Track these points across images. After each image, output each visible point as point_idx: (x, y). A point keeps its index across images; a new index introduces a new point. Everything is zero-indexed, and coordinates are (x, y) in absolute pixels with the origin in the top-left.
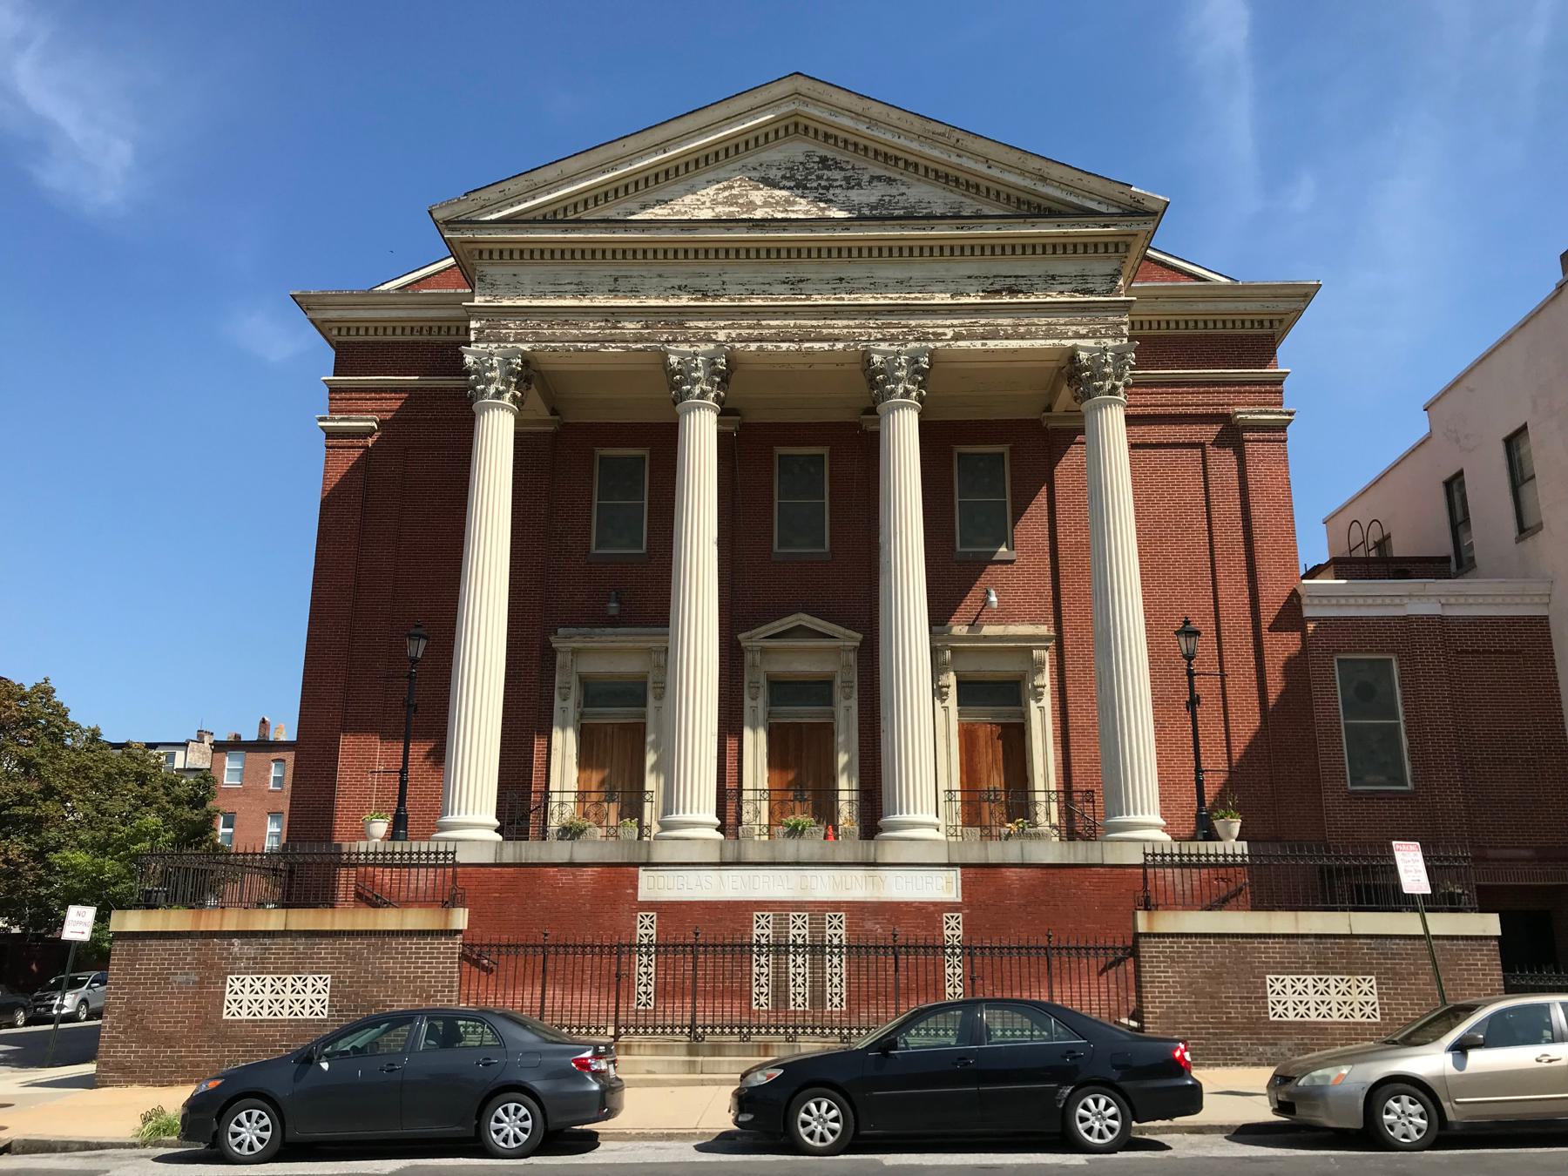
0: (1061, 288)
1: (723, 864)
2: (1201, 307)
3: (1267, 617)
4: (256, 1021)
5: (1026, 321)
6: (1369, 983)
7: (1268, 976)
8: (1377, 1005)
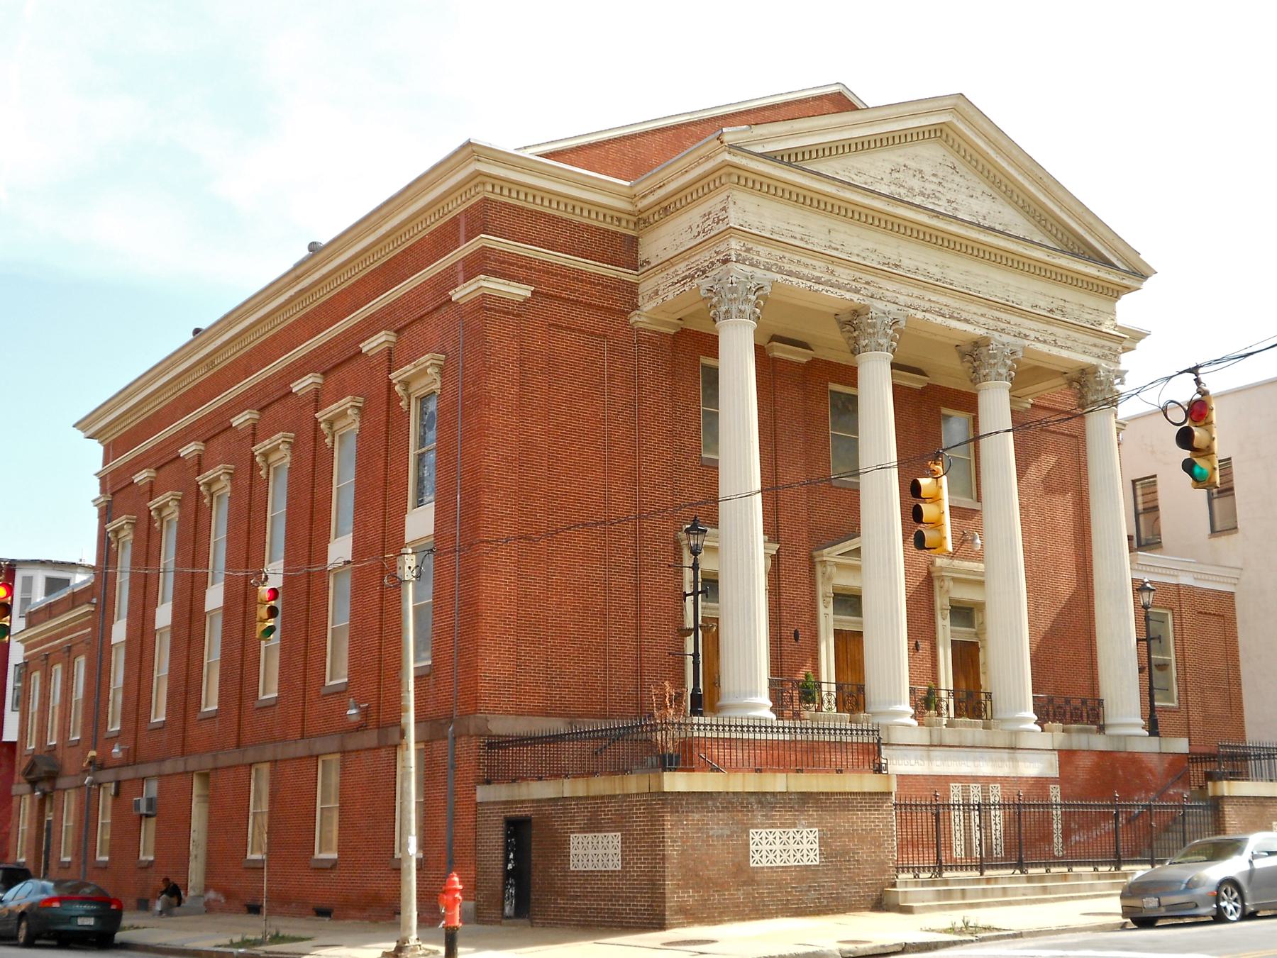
4: (772, 868)
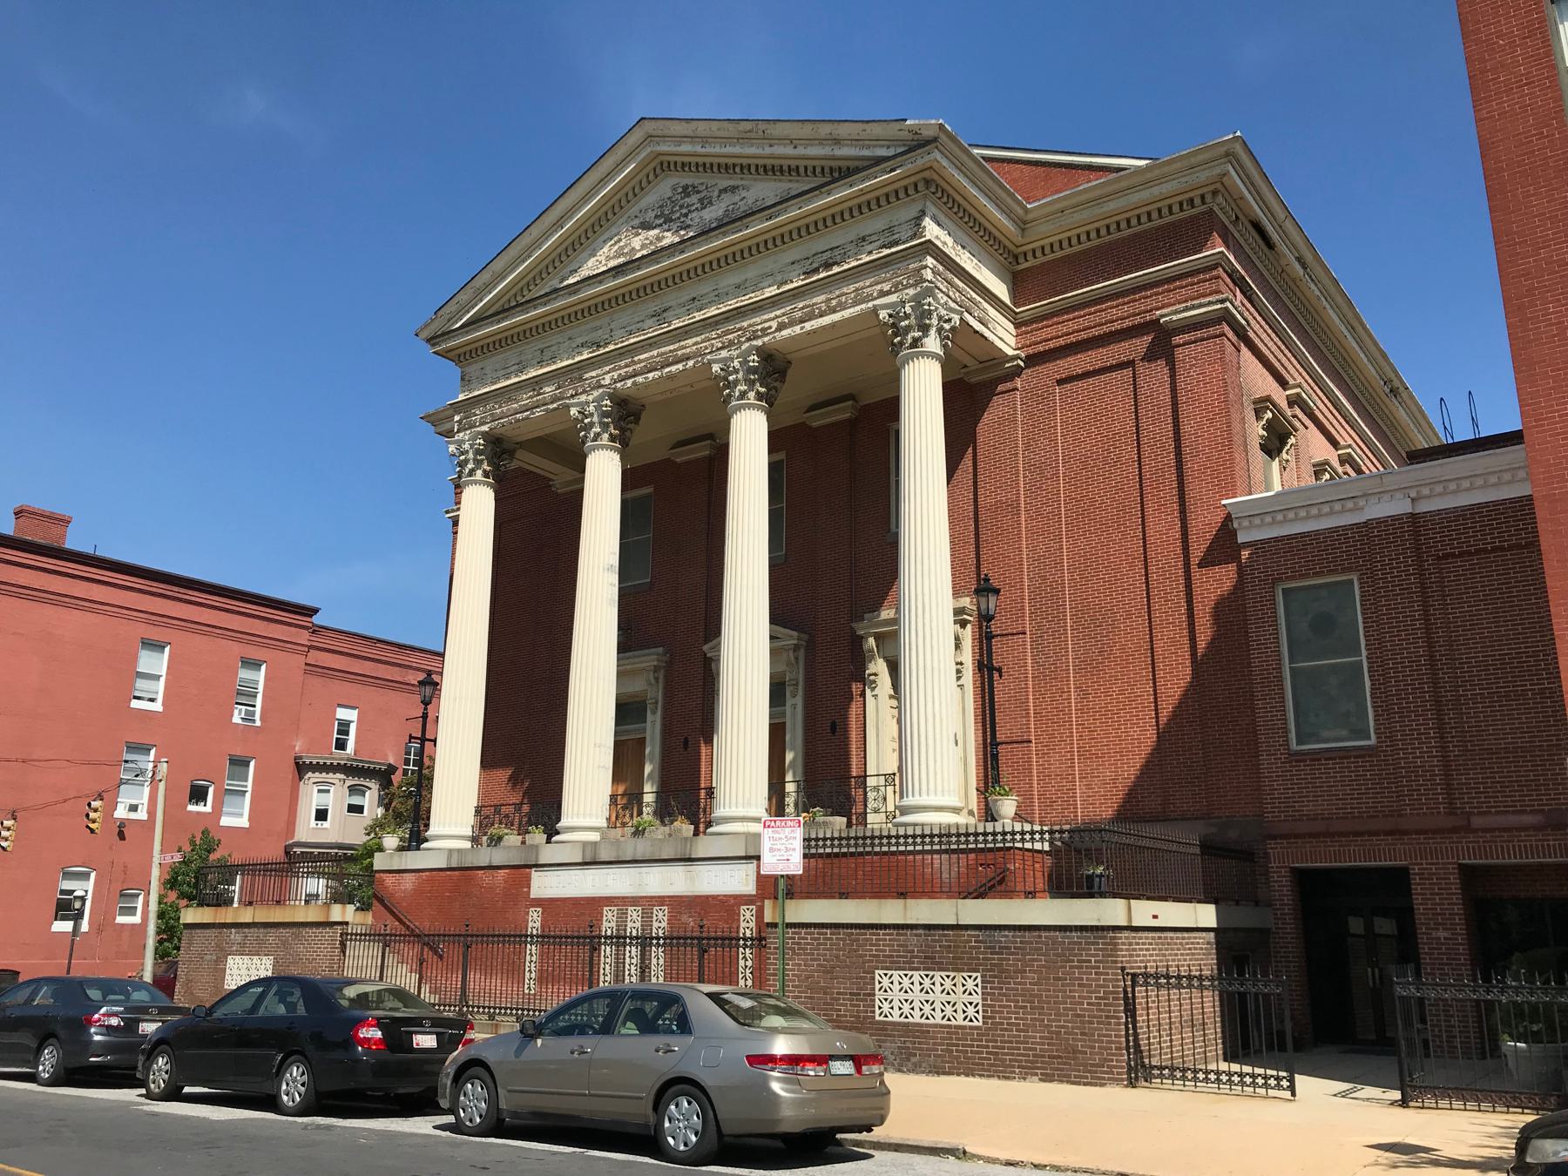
0: (869, 248)
1: (585, 864)
2: (1112, 206)
3: (1197, 553)
5: (837, 293)
6: (973, 981)
7: (877, 971)
8: (980, 1007)
